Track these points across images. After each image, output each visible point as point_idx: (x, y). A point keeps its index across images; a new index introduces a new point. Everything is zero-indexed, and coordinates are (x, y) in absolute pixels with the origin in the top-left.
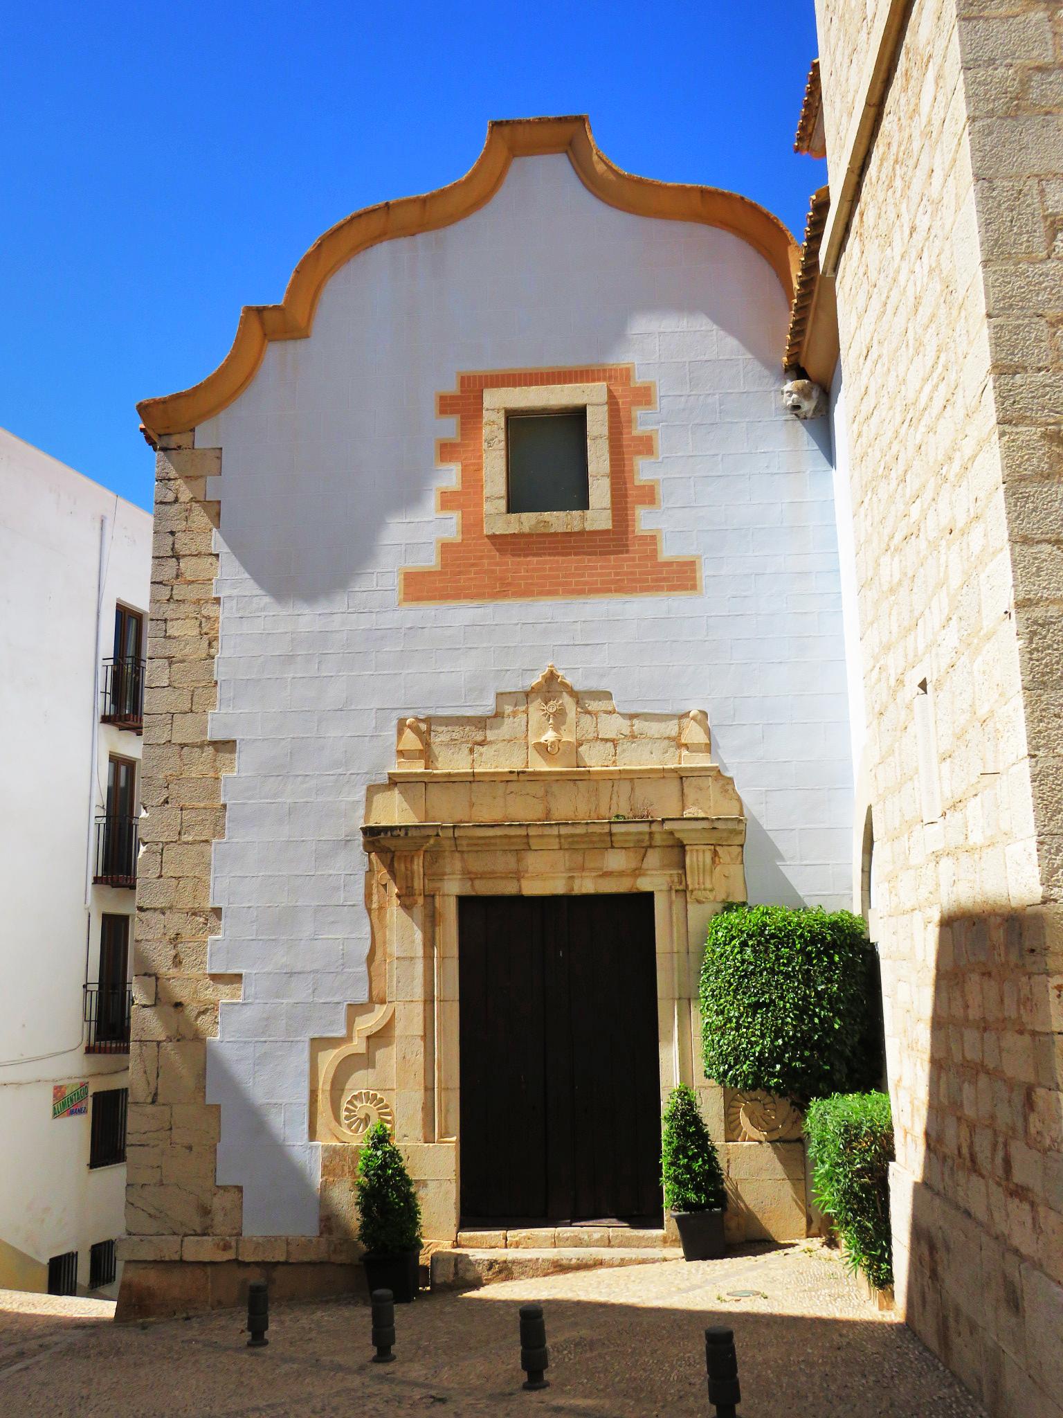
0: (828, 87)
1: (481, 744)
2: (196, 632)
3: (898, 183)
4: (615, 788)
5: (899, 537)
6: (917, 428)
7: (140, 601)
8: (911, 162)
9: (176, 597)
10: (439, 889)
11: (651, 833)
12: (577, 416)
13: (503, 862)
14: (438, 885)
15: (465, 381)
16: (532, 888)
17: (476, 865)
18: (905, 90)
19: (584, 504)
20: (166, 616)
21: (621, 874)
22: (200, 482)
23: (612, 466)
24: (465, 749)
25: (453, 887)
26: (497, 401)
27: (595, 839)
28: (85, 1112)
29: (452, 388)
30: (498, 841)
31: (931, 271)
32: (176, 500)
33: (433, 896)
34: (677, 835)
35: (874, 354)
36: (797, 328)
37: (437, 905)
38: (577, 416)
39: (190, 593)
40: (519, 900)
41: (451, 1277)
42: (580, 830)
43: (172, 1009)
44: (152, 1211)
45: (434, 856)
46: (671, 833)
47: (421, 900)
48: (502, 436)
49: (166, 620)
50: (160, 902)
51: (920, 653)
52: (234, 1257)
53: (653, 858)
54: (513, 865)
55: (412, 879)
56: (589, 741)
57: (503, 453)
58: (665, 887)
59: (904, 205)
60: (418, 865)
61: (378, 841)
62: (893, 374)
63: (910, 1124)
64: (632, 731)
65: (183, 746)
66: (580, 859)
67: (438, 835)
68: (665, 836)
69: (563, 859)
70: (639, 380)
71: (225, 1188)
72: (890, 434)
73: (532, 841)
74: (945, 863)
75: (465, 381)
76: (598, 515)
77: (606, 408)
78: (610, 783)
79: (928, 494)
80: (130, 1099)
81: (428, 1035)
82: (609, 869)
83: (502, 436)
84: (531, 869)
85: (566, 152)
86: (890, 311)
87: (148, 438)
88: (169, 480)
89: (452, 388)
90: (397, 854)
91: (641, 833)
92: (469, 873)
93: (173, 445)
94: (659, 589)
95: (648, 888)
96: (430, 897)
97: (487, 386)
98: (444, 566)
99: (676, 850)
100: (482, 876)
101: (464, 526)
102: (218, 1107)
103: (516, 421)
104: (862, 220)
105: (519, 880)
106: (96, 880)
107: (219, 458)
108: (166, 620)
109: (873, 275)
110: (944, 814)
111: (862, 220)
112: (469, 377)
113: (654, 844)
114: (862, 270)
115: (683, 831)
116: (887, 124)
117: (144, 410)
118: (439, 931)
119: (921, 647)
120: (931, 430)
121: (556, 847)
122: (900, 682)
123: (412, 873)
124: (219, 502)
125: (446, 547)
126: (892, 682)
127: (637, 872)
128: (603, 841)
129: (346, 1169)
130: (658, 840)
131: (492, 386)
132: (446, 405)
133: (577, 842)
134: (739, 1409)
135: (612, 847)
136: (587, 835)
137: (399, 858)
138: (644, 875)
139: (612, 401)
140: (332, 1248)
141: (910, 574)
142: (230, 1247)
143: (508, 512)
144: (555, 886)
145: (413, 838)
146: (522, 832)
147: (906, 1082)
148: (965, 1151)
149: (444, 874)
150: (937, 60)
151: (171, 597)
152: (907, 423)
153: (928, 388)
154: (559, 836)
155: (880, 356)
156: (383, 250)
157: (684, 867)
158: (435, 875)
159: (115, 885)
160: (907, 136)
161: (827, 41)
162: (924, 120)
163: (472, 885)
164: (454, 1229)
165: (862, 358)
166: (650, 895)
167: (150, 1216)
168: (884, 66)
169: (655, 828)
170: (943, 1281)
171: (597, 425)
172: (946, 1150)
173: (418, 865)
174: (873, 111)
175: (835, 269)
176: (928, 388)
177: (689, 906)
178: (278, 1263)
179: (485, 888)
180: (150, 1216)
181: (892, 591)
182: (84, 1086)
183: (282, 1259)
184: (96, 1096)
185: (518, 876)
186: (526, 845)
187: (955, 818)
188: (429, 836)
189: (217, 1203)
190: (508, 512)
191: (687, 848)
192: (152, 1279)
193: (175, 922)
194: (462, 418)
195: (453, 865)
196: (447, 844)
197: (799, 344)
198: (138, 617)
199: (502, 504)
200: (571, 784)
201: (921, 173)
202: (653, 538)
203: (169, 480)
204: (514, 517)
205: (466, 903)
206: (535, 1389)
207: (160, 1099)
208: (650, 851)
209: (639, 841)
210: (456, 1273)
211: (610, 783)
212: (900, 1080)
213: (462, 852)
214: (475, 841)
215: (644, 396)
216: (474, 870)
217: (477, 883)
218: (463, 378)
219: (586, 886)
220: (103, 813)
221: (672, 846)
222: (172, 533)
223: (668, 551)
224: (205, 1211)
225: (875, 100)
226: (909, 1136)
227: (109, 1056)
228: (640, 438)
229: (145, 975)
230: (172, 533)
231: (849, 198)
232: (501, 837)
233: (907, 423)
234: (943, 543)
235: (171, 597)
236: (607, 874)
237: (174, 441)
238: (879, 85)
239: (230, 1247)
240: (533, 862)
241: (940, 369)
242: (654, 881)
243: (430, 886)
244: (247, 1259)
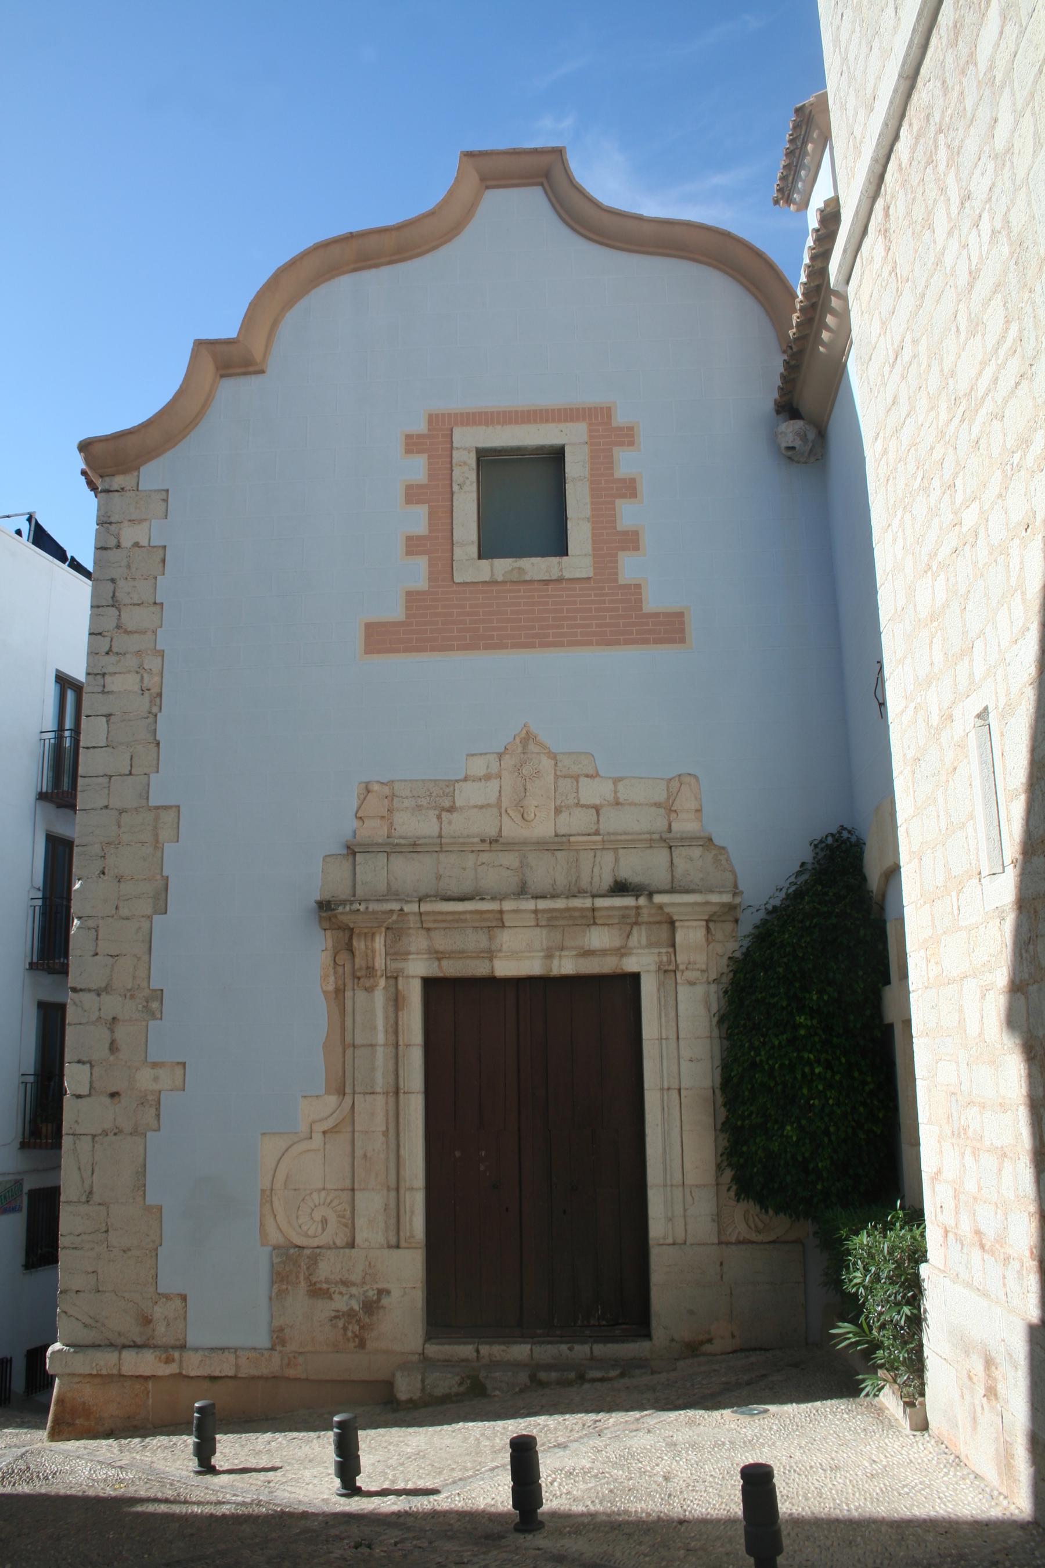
0: (838, 89)
1: (451, 810)
2: (137, 688)
3: (942, 154)
4: (598, 859)
5: (944, 552)
7: (78, 672)
9: (115, 649)
10: (402, 970)
12: (556, 456)
13: (474, 940)
14: (401, 965)
15: (433, 419)
16: (504, 968)
17: (442, 942)
18: (954, 43)
19: (562, 550)
20: (104, 671)
21: (604, 952)
22: (146, 524)
23: (593, 510)
24: (432, 814)
25: (418, 968)
26: (470, 439)
27: (577, 914)
28: (20, 1210)
29: (420, 427)
30: (468, 916)
31: (994, 233)
32: (118, 546)
33: (396, 978)
34: (667, 910)
35: (907, 355)
36: (793, 363)
37: (400, 987)
40: (492, 981)
42: (560, 904)
43: (108, 1100)
44: (88, 1321)
45: (396, 931)
46: (661, 907)
47: (382, 982)
48: (473, 476)
49: (104, 675)
50: (97, 983)
51: (978, 677)
52: (177, 1371)
54: (484, 943)
55: (373, 958)
56: (568, 807)
58: (653, 967)
60: (379, 943)
61: (335, 916)
63: (952, 1223)
65: (121, 811)
67: (402, 910)
68: (653, 911)
69: (539, 937)
70: (620, 419)
71: (168, 1297)
73: (506, 917)
75: (433, 419)
77: (586, 449)
78: (592, 854)
80: (62, 1198)
82: (592, 948)
84: (505, 947)
85: (542, 184)
88: (110, 523)
89: (420, 427)
90: (357, 931)
91: (626, 908)
92: (437, 952)
93: (115, 487)
96: (394, 978)
98: (408, 616)
101: (431, 573)
104: (887, 215)
105: (491, 959)
106: (32, 966)
107: (166, 500)
108: (104, 675)
111: (887, 215)
112: (437, 415)
113: (640, 919)
114: (887, 268)
115: (673, 904)
118: (403, 1016)
123: (373, 951)
124: (164, 547)
125: (412, 597)
126: (935, 720)
127: (622, 952)
128: (583, 917)
130: (645, 917)
131: (462, 424)
133: (556, 918)
134: (780, 1560)
135: (595, 924)
136: (567, 909)
137: (359, 935)
138: (630, 954)
142: (173, 1360)
143: (480, 557)
144: (531, 967)
145: (374, 912)
146: (493, 906)
149: (409, 953)
153: (989, 371)
155: (915, 356)
156: (345, 283)
157: (673, 946)
158: (396, 953)
159: (51, 971)
161: (837, 41)
162: (983, 66)
163: (440, 967)
166: (635, 979)
167: (85, 1326)
170: (1007, 1402)
171: (575, 467)
172: (1010, 1251)
173: (379, 943)
176: (989, 371)
177: (679, 988)
178: (227, 1377)
179: (451, 969)
180: (85, 1326)
181: (933, 617)
182: (19, 1183)
183: (231, 1373)
184: (32, 1194)
185: (490, 955)
186: (499, 921)
188: (392, 911)
189: (158, 1312)
190: (480, 557)
191: (677, 924)
192: (88, 1393)
193: (111, 1004)
194: (429, 457)
195: (417, 942)
196: (413, 922)
198: (78, 688)
199: (474, 550)
202: (638, 586)
203: (110, 523)
204: (485, 563)
206: (529, 1531)
207: (96, 1198)
208: (635, 929)
209: (623, 917)
210: (423, 1389)
211: (592, 854)
212: (939, 1172)
213: (428, 930)
214: (440, 918)
215: (627, 436)
216: (441, 948)
217: (444, 963)
219: (566, 966)
220: (40, 895)
221: (659, 923)
222: (113, 581)
224: (147, 1321)
226: (951, 1236)
228: (623, 481)
229: (79, 1062)
230: (113, 581)
232: (471, 912)
233: (956, 421)
234: (1017, 541)
237: (118, 481)
239: (173, 1360)
240: (507, 939)
241: (1009, 341)
243: (393, 966)
244: (192, 1374)
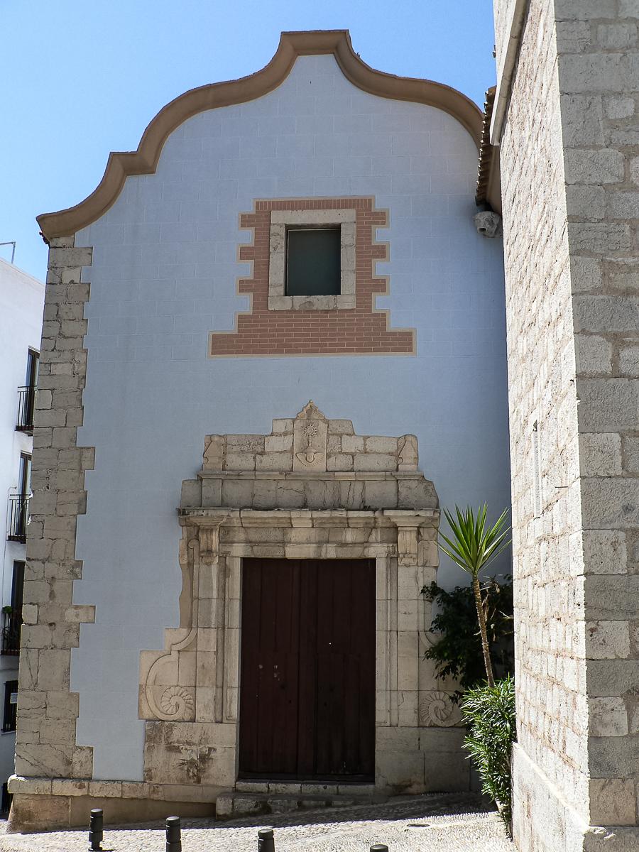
3: (528, 90)
4: (352, 486)
6: (535, 252)
8: (533, 77)
9: (57, 348)
11: (375, 518)
12: (335, 231)
15: (259, 205)
17: (254, 536)
19: (337, 291)
25: (239, 551)
26: (281, 219)
27: (337, 521)
29: (251, 210)
30: (270, 520)
34: (394, 520)
38: (335, 231)
39: (68, 344)
40: (285, 561)
41: (230, 811)
43: (48, 627)
46: (389, 518)
47: (217, 560)
49: (50, 364)
53: (376, 535)
54: (280, 538)
56: (335, 454)
57: (283, 255)
59: (530, 104)
62: (525, 214)
64: (365, 449)
66: (326, 534)
72: (523, 255)
74: (544, 544)
75: (259, 205)
76: (347, 298)
79: (540, 298)
81: (220, 651)
83: (283, 243)
86: (524, 173)
87: (44, 239)
89: (251, 210)
91: (368, 518)
92: (251, 542)
94: (387, 350)
95: (372, 555)
97: (274, 209)
99: (393, 530)
100: (258, 543)
102: (78, 695)
103: (293, 233)
107: (91, 254)
108: (50, 364)
109: (516, 147)
110: (543, 512)
112: (261, 202)
115: (396, 517)
116: (523, 52)
117: (41, 219)
119: (535, 398)
120: (541, 255)
121: (311, 526)
122: (526, 422)
125: (242, 319)
127: (366, 543)
129: (163, 738)
130: (380, 522)
131: (277, 209)
132: (246, 221)
135: (349, 527)
136: (331, 518)
139: (358, 222)
140: (152, 789)
141: (531, 350)
142: (84, 787)
147: (523, 690)
148: (546, 734)
150: (544, 13)
151: (55, 348)
152: (530, 249)
153: (540, 227)
154: (312, 519)
160: (531, 60)
162: (539, 51)
164: (234, 780)
165: (511, 202)
168: (520, 13)
169: (377, 514)
171: (347, 238)
174: (515, 41)
175: (500, 140)
179: (260, 552)
185: (284, 543)
187: (548, 515)
188: (223, 516)
189: (76, 758)
190: (286, 294)
197: (485, 187)
199: (281, 290)
200: (321, 483)
201: (537, 85)
202: (384, 315)
205: (246, 562)
214: (253, 521)
215: (381, 218)
218: (257, 203)
219: (331, 552)
223: (394, 325)
225: (516, 34)
227: (12, 657)
231: (505, 95)
233: (530, 249)
235: (55, 348)
236: (343, 544)
238: (518, 25)
239: (84, 787)
242: (377, 551)
